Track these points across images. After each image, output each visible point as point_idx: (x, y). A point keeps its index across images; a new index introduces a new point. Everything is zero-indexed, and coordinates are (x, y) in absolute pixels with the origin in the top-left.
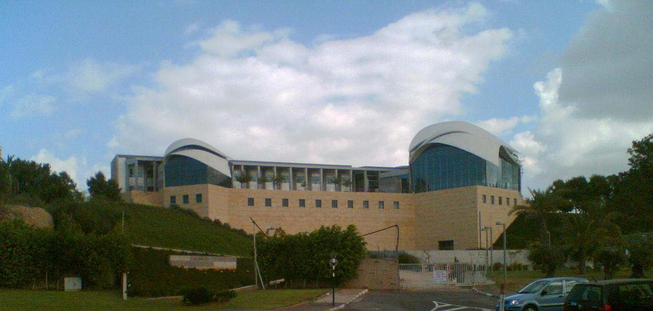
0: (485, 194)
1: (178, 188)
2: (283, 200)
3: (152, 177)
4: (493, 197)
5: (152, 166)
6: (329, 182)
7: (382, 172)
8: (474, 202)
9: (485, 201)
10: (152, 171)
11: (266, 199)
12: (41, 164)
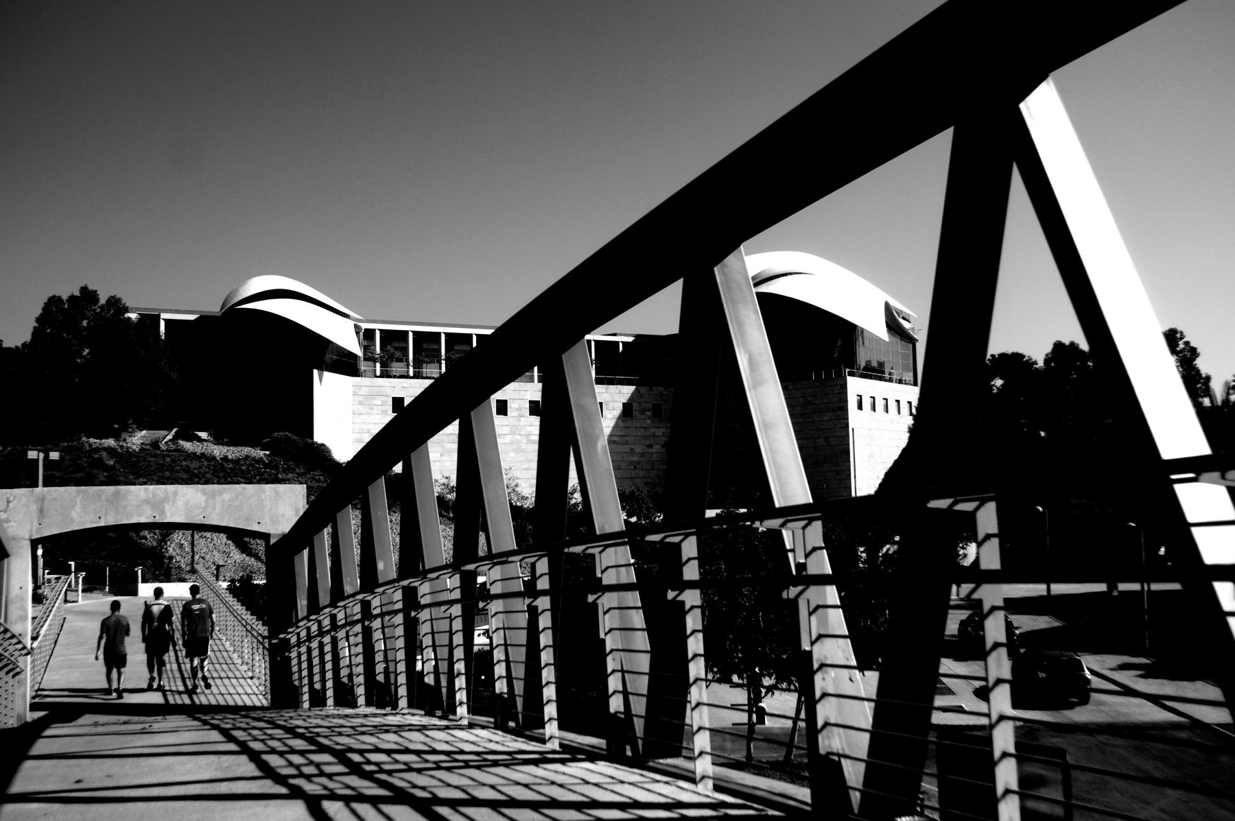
9: (860, 407)
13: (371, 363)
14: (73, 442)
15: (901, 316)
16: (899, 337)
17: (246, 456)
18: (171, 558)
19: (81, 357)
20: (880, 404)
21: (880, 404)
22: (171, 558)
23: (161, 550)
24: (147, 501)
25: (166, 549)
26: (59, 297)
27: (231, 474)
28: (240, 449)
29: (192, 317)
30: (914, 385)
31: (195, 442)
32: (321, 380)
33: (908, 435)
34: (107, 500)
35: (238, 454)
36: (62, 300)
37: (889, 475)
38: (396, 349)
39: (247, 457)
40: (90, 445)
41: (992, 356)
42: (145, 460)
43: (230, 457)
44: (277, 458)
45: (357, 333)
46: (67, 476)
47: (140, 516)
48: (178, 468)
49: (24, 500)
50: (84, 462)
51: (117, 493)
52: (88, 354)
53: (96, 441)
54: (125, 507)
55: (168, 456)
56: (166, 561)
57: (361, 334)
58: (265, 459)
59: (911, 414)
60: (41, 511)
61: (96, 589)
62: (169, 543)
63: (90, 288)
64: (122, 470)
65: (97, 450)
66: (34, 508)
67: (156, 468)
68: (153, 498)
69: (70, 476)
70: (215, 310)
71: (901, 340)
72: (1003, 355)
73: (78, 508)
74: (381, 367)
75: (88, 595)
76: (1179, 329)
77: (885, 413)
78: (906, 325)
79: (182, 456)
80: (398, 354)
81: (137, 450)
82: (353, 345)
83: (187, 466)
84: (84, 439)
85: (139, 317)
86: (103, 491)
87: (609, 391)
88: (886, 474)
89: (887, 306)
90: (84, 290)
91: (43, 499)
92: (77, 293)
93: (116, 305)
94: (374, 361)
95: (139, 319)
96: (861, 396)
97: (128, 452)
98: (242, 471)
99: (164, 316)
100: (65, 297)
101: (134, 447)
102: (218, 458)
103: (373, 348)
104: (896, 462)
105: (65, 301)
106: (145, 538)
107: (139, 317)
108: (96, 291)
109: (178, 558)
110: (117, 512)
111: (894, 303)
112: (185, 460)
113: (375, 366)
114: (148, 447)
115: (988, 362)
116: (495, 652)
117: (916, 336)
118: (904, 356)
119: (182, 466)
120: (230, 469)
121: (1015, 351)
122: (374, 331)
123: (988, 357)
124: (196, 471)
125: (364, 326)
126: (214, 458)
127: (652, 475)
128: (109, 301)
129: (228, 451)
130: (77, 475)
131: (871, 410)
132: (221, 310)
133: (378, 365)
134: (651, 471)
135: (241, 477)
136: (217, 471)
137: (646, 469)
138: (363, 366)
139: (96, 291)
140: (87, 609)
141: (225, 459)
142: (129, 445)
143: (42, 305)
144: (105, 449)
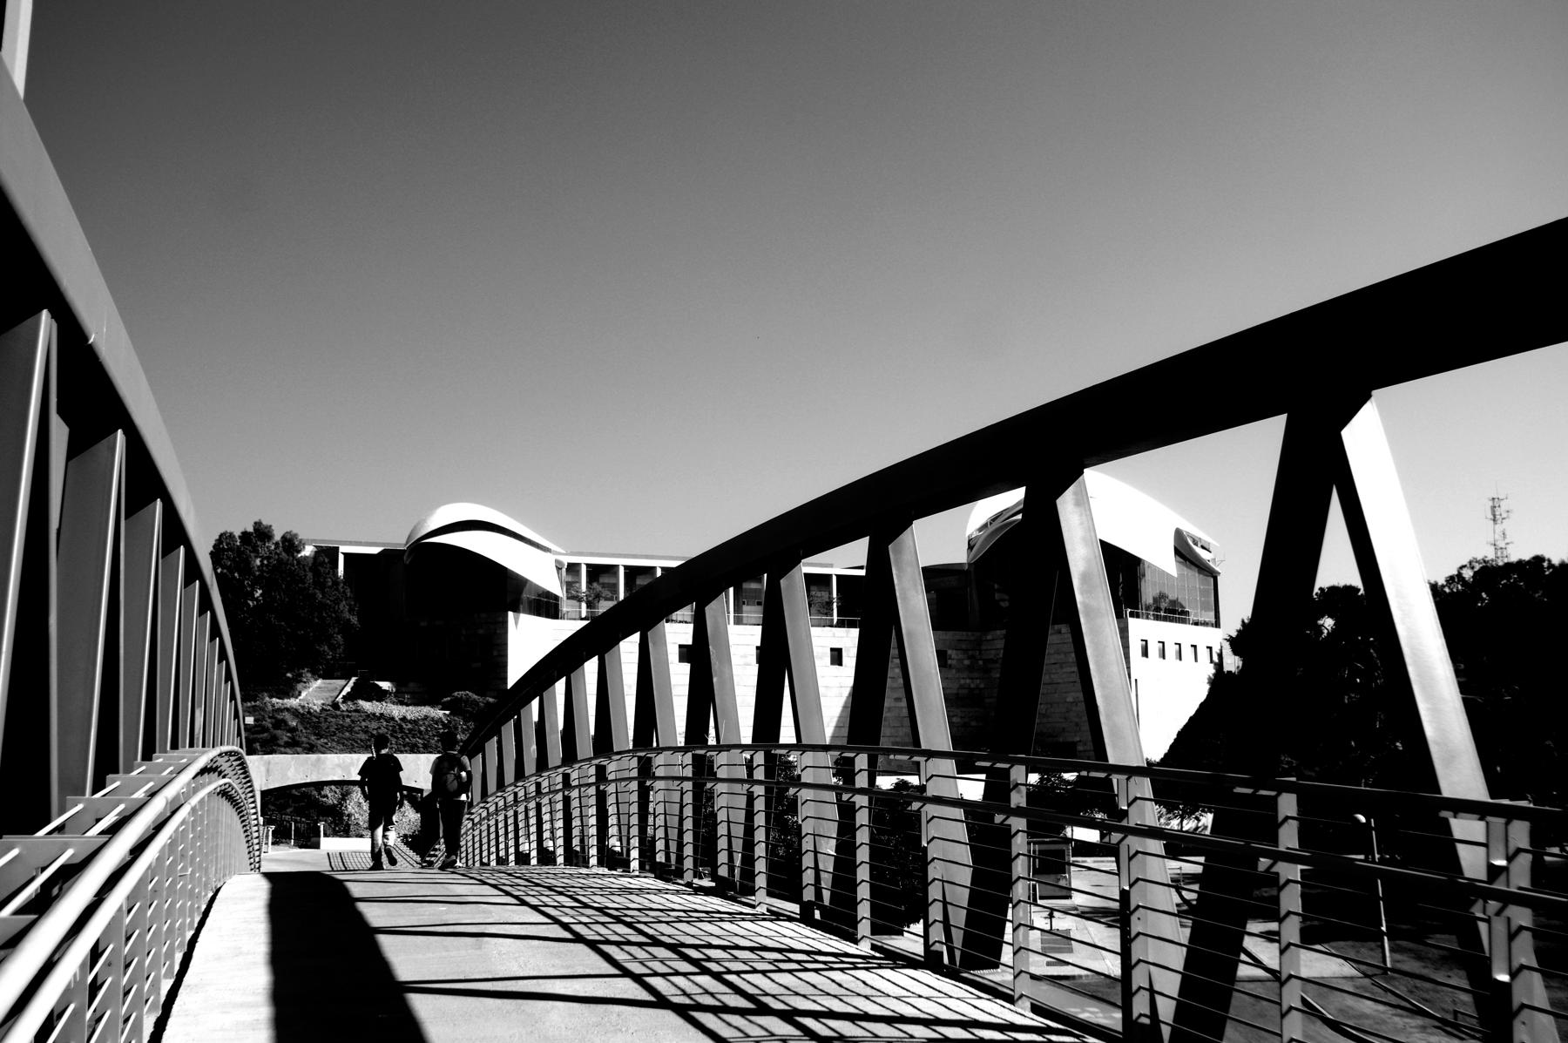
4: (1195, 647)
9: (1145, 653)
13: (574, 602)
14: (255, 702)
15: (1199, 545)
16: (1196, 569)
17: (426, 716)
18: (349, 816)
19: (253, 599)
20: (1171, 651)
21: (1171, 651)
22: (349, 816)
23: (341, 808)
24: (339, 766)
25: (346, 807)
26: (231, 534)
27: (409, 735)
28: (419, 708)
29: (375, 550)
30: (1216, 627)
31: (374, 702)
32: (516, 623)
33: (1208, 687)
34: (312, 765)
35: (417, 715)
36: (234, 536)
37: (1182, 735)
38: (604, 586)
39: (426, 717)
40: (273, 706)
41: (1321, 589)
42: (326, 719)
43: (409, 718)
44: (456, 718)
45: (559, 569)
46: (252, 736)
47: (1082, 594)
48: (357, 729)
49: (256, 764)
50: (268, 723)
51: (319, 759)
52: (261, 595)
53: (278, 700)
54: (324, 769)
55: (348, 716)
56: (346, 818)
57: (564, 570)
58: (444, 720)
59: (1212, 661)
60: (268, 771)
61: (282, 843)
62: (348, 801)
63: (265, 523)
64: (304, 731)
65: (280, 710)
66: (263, 769)
67: (336, 729)
68: (344, 762)
69: (255, 736)
70: (400, 545)
71: (1199, 573)
72: (1333, 589)
73: (292, 769)
74: (588, 607)
75: (276, 847)
76: (1547, 556)
77: (1162, 659)
78: (1203, 554)
79: (361, 716)
80: (606, 593)
81: (318, 711)
82: (551, 582)
83: (366, 727)
84: (267, 699)
85: (315, 550)
86: (309, 758)
87: (849, 635)
88: (1179, 734)
89: (1179, 534)
90: (258, 525)
91: (269, 763)
92: (250, 529)
93: (290, 544)
94: (580, 600)
95: (316, 552)
96: (1146, 641)
97: (309, 712)
98: (420, 732)
99: (343, 549)
100: (237, 533)
101: (315, 708)
102: (397, 719)
103: (577, 585)
104: (1191, 719)
105: (237, 537)
106: (326, 796)
107: (315, 550)
108: (271, 526)
109: (357, 816)
110: (319, 773)
111: (1189, 528)
112: (364, 720)
113: (580, 607)
114: (329, 708)
115: (1315, 597)
116: (532, 853)
117: (1217, 569)
118: (1203, 593)
119: (361, 727)
120: (408, 729)
121: (1348, 584)
122: (578, 565)
123: (1316, 590)
124: (375, 732)
125: (567, 560)
126: (393, 719)
127: (901, 734)
128: (284, 537)
129: (407, 711)
130: (261, 736)
131: (1160, 656)
132: (407, 543)
133: (584, 605)
134: (900, 729)
135: (419, 738)
136: (396, 732)
137: (894, 727)
138: (566, 606)
139: (271, 526)
140: (278, 857)
141: (404, 719)
142: (310, 705)
143: (213, 543)
144: (288, 710)
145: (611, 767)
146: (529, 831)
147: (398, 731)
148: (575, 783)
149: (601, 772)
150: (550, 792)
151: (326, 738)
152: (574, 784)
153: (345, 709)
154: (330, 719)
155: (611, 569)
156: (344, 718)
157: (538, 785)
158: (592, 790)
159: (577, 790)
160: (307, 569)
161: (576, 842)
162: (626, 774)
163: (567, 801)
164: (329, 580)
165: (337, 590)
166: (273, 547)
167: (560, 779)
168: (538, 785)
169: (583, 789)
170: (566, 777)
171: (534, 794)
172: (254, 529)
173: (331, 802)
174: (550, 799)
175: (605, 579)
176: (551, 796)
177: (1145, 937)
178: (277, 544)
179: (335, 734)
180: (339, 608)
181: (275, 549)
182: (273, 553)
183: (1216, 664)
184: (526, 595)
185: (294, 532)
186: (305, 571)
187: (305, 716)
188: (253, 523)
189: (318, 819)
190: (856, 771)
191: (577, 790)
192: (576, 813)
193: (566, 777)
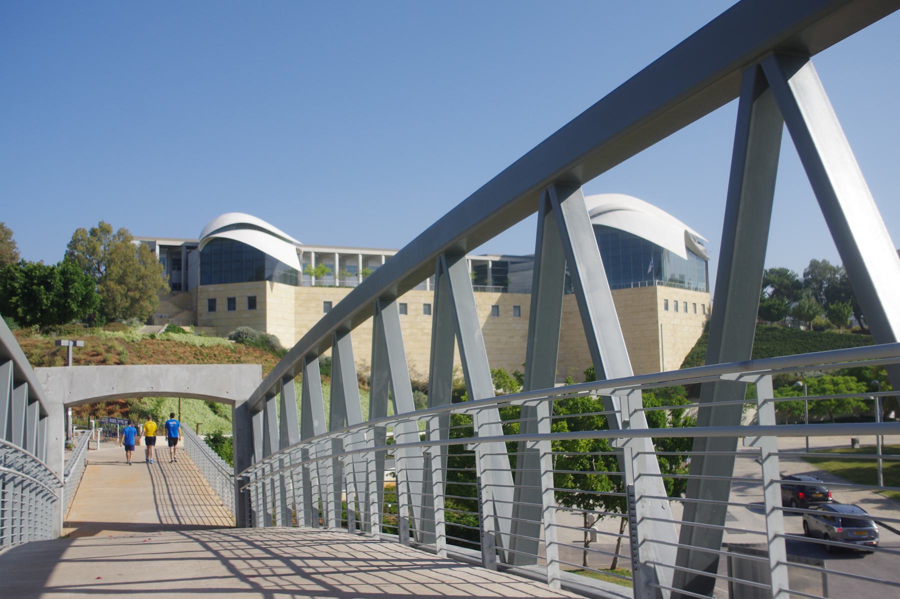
0: (666, 299)
1: (221, 287)
2: (325, 302)
3: (179, 269)
4: (695, 304)
5: (179, 253)
6: (392, 489)
7: (512, 263)
8: (654, 309)
9: (666, 308)
10: (180, 260)
11: (234, 309)
12: (17, 249)
13: (308, 277)
20: (681, 306)
21: (681, 306)
25: (160, 411)
26: (84, 230)
32: (272, 288)
35: (212, 343)
36: (86, 231)
39: (218, 345)
43: (206, 345)
45: (298, 254)
55: (162, 344)
59: (704, 313)
61: (110, 440)
62: (162, 407)
64: (128, 354)
71: (697, 258)
75: (104, 444)
80: (328, 270)
92: (96, 226)
96: (667, 300)
97: (133, 341)
100: (88, 229)
101: (138, 338)
102: (198, 346)
106: (145, 403)
108: (110, 225)
113: (311, 279)
117: (708, 256)
119: (172, 351)
121: (782, 267)
122: (309, 253)
125: (303, 249)
126: (194, 346)
129: (205, 340)
133: (313, 278)
138: (302, 279)
145: (348, 441)
146: (274, 492)
147: (199, 354)
148: (313, 457)
149: (338, 445)
150: (291, 466)
151: (145, 359)
152: (312, 457)
153: (159, 339)
154: (148, 346)
155: (331, 256)
156: (158, 344)
157: (281, 461)
158: (329, 462)
159: (315, 463)
160: (135, 252)
161: (315, 498)
162: (363, 446)
163: (306, 473)
164: (150, 259)
165: (155, 266)
166: (112, 238)
167: (299, 455)
168: (281, 461)
169: (320, 462)
170: (305, 453)
171: (278, 468)
172: (99, 226)
173: (148, 407)
174: (291, 472)
175: (326, 262)
176: (292, 469)
177: (643, 455)
178: (114, 236)
179: (152, 356)
180: (156, 278)
181: (114, 239)
182: (112, 242)
183: (707, 315)
184: (278, 272)
185: (126, 228)
186: (133, 253)
187: (130, 344)
188: (98, 223)
189: (138, 421)
190: (539, 419)
191: (315, 463)
192: (315, 482)
193: (305, 453)
